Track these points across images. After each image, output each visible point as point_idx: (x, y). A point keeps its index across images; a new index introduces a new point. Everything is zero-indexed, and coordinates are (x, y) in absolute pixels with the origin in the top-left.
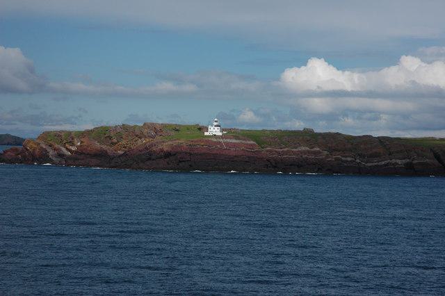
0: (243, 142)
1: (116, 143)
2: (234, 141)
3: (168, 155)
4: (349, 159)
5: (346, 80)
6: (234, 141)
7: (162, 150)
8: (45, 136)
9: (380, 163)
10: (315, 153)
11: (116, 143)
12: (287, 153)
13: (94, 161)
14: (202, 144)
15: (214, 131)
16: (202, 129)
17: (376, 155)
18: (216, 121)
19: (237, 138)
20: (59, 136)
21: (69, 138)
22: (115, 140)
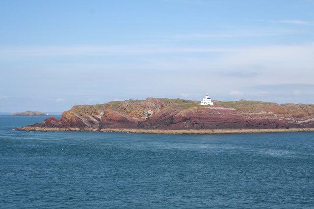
0: (229, 109)
1: (130, 112)
2: (223, 108)
3: (185, 119)
4: (289, 119)
5: (210, 147)
6: (223, 108)
7: (180, 116)
8: (76, 108)
9: (305, 121)
10: (270, 115)
11: (130, 112)
12: (255, 116)
13: (116, 124)
14: (205, 111)
15: (206, 102)
16: (200, 102)
17: (301, 116)
18: (207, 95)
19: (223, 106)
20: (85, 108)
21: (92, 110)
22: (128, 110)
